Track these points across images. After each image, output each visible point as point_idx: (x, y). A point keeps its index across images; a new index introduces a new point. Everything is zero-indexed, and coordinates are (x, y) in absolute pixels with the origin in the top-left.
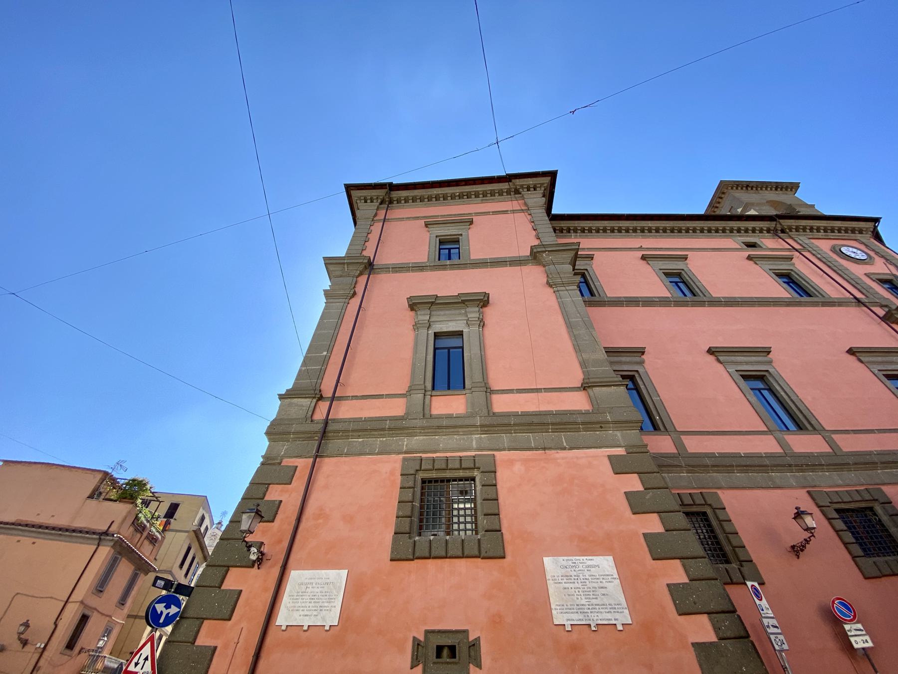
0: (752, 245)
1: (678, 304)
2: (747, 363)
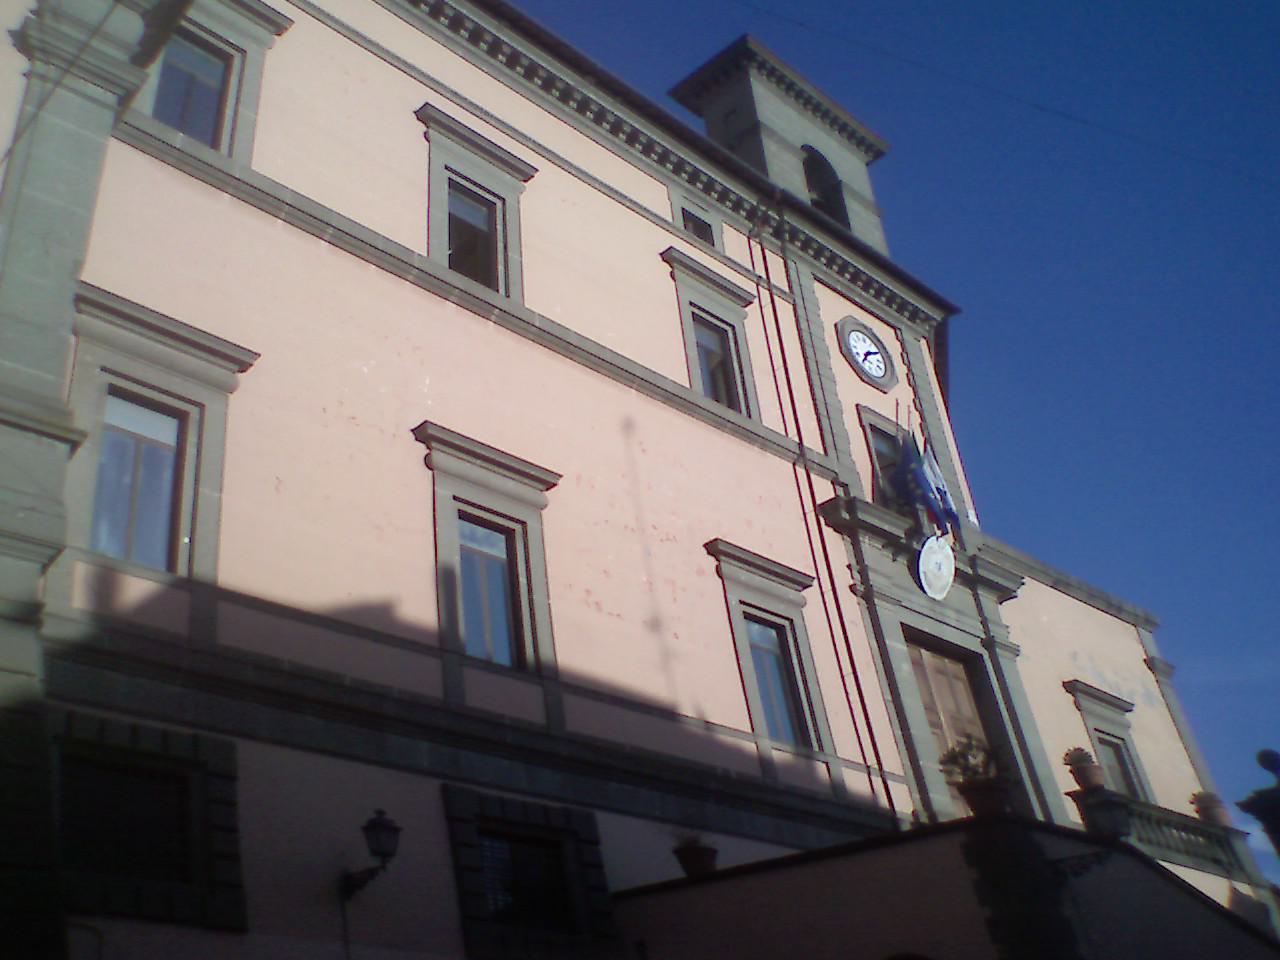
0: (701, 231)
1: (427, 281)
2: (171, 367)
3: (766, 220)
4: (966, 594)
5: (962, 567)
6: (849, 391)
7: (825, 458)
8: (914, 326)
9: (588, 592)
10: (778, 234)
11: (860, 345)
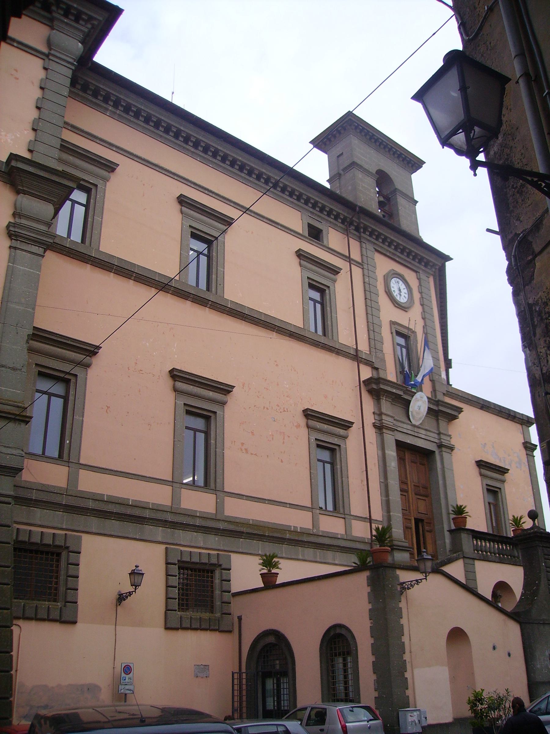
0: (315, 234)
3: (351, 223)
4: (433, 422)
5: (432, 406)
6: (388, 313)
7: (323, 337)
8: (427, 270)
9: (243, 444)
10: (357, 229)
11: (396, 285)
